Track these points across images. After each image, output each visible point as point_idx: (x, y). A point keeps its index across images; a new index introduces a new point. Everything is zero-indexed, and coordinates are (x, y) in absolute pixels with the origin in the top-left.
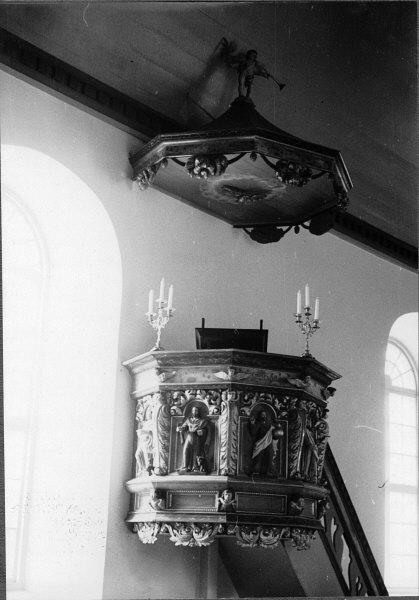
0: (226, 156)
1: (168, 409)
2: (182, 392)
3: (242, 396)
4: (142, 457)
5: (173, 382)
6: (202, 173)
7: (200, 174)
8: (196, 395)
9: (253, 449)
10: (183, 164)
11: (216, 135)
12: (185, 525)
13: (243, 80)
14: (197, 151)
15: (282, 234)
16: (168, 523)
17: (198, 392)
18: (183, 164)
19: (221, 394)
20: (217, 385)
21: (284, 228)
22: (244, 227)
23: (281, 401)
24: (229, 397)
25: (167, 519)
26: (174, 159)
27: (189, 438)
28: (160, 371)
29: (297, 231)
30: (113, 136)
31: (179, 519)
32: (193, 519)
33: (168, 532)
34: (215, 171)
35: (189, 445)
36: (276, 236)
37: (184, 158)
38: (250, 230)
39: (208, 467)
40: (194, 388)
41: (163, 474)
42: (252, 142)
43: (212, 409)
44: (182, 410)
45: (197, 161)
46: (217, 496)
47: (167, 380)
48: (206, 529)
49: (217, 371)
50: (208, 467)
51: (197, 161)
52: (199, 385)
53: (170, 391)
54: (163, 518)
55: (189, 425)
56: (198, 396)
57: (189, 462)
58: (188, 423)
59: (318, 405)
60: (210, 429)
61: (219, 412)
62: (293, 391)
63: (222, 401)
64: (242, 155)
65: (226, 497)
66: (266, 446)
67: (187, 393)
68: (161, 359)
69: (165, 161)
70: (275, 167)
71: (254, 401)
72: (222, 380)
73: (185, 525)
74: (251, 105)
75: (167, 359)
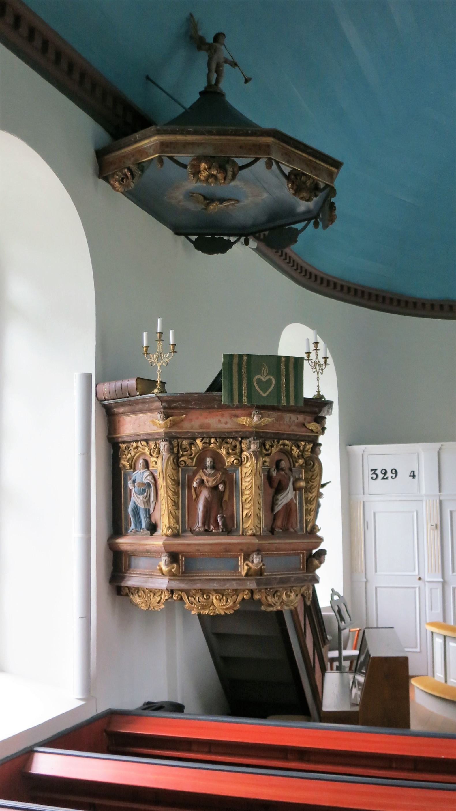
0: (236, 160)
1: (177, 463)
2: (193, 439)
3: (263, 445)
4: (136, 510)
5: (181, 428)
6: (210, 180)
7: (207, 180)
8: (210, 443)
9: (273, 504)
10: (185, 166)
11: (225, 133)
12: (203, 592)
13: (214, 66)
14: (200, 151)
15: (229, 245)
16: (182, 590)
17: (213, 440)
18: (185, 166)
19: (241, 443)
20: (237, 432)
21: (232, 239)
22: (186, 235)
23: (298, 447)
24: (253, 447)
25: (183, 586)
26: (171, 158)
27: (205, 494)
28: (167, 416)
29: (247, 243)
30: (82, 129)
31: (198, 586)
32: (215, 586)
33: (181, 599)
34: (225, 179)
35: (206, 500)
36: (223, 247)
37: (186, 158)
38: (194, 238)
39: (229, 528)
40: (207, 436)
41: (176, 535)
42: (268, 146)
43: (231, 460)
44: (192, 459)
45: (203, 165)
46: (241, 559)
47: (174, 424)
48: (227, 596)
49: (237, 416)
50: (229, 528)
51: (203, 165)
52: (213, 433)
53: (177, 438)
54: (175, 585)
55: (205, 478)
56: (212, 445)
57: (206, 520)
58: (201, 475)
59: (216, 438)
60: (229, 481)
61: (241, 463)
62: (309, 436)
63: (242, 451)
64: (257, 160)
65: (255, 561)
66: (288, 500)
67: (198, 441)
68: (167, 402)
69: (160, 160)
70: (288, 177)
71: (274, 450)
72: (243, 426)
73: (203, 592)
74: (221, 95)
75: (174, 401)
